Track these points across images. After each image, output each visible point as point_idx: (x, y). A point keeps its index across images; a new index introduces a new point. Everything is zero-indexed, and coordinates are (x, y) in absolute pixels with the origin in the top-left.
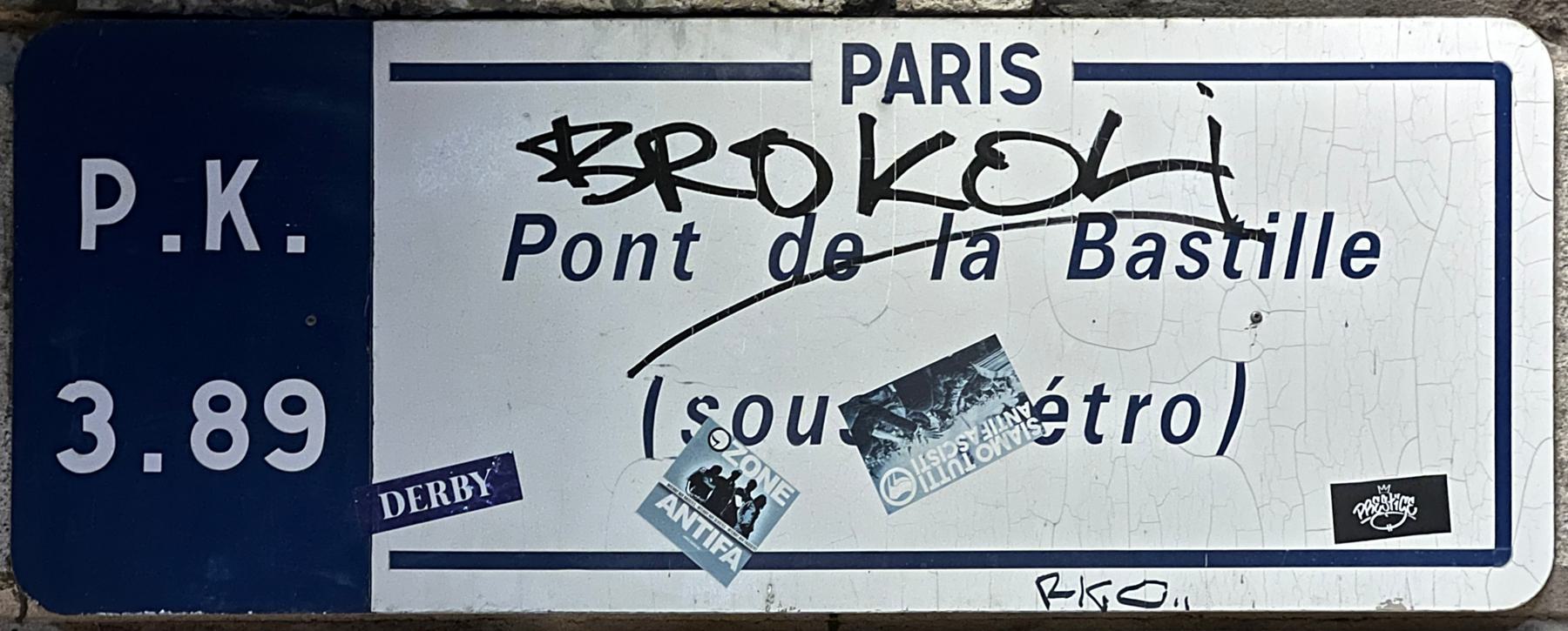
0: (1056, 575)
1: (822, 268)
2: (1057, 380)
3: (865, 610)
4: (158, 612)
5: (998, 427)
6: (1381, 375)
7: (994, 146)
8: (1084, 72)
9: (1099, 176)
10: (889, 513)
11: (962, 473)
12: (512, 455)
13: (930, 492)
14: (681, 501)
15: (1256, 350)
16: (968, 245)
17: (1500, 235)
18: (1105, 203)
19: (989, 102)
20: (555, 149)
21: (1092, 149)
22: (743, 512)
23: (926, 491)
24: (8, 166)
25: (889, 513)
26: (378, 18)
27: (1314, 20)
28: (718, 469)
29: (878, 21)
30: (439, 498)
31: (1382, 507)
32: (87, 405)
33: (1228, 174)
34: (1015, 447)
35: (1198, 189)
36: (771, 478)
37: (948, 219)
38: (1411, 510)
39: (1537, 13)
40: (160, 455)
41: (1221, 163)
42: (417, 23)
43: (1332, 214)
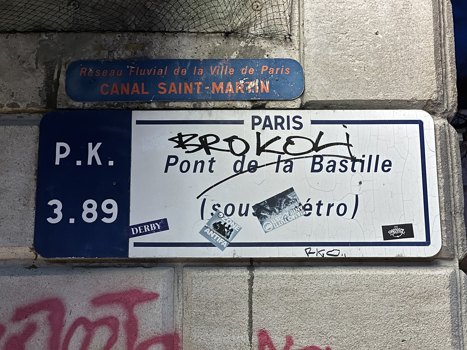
0: (310, 248)
1: (247, 169)
2: (309, 199)
3: (260, 257)
4: (72, 257)
5: (294, 212)
6: (394, 198)
7: (291, 139)
8: (313, 122)
9: (318, 146)
10: (266, 233)
11: (285, 223)
12: (166, 219)
13: (276, 228)
14: (211, 230)
15: (361, 191)
16: (285, 163)
17: (422, 161)
18: (320, 153)
19: (289, 129)
20: (178, 140)
21: (316, 140)
22: (227, 233)
23: (275, 227)
24: (37, 144)
25: (266, 233)
26: (133, 110)
27: (372, 110)
28: (220, 222)
29: (261, 111)
30: (147, 229)
31: (396, 231)
32: (55, 206)
33: (351, 146)
34: (298, 217)
35: (344, 149)
36: (234, 224)
37: (279, 157)
38: (403, 232)
39: (429, 109)
40: (74, 219)
41: (350, 143)
42: (143, 111)
43: (379, 155)
